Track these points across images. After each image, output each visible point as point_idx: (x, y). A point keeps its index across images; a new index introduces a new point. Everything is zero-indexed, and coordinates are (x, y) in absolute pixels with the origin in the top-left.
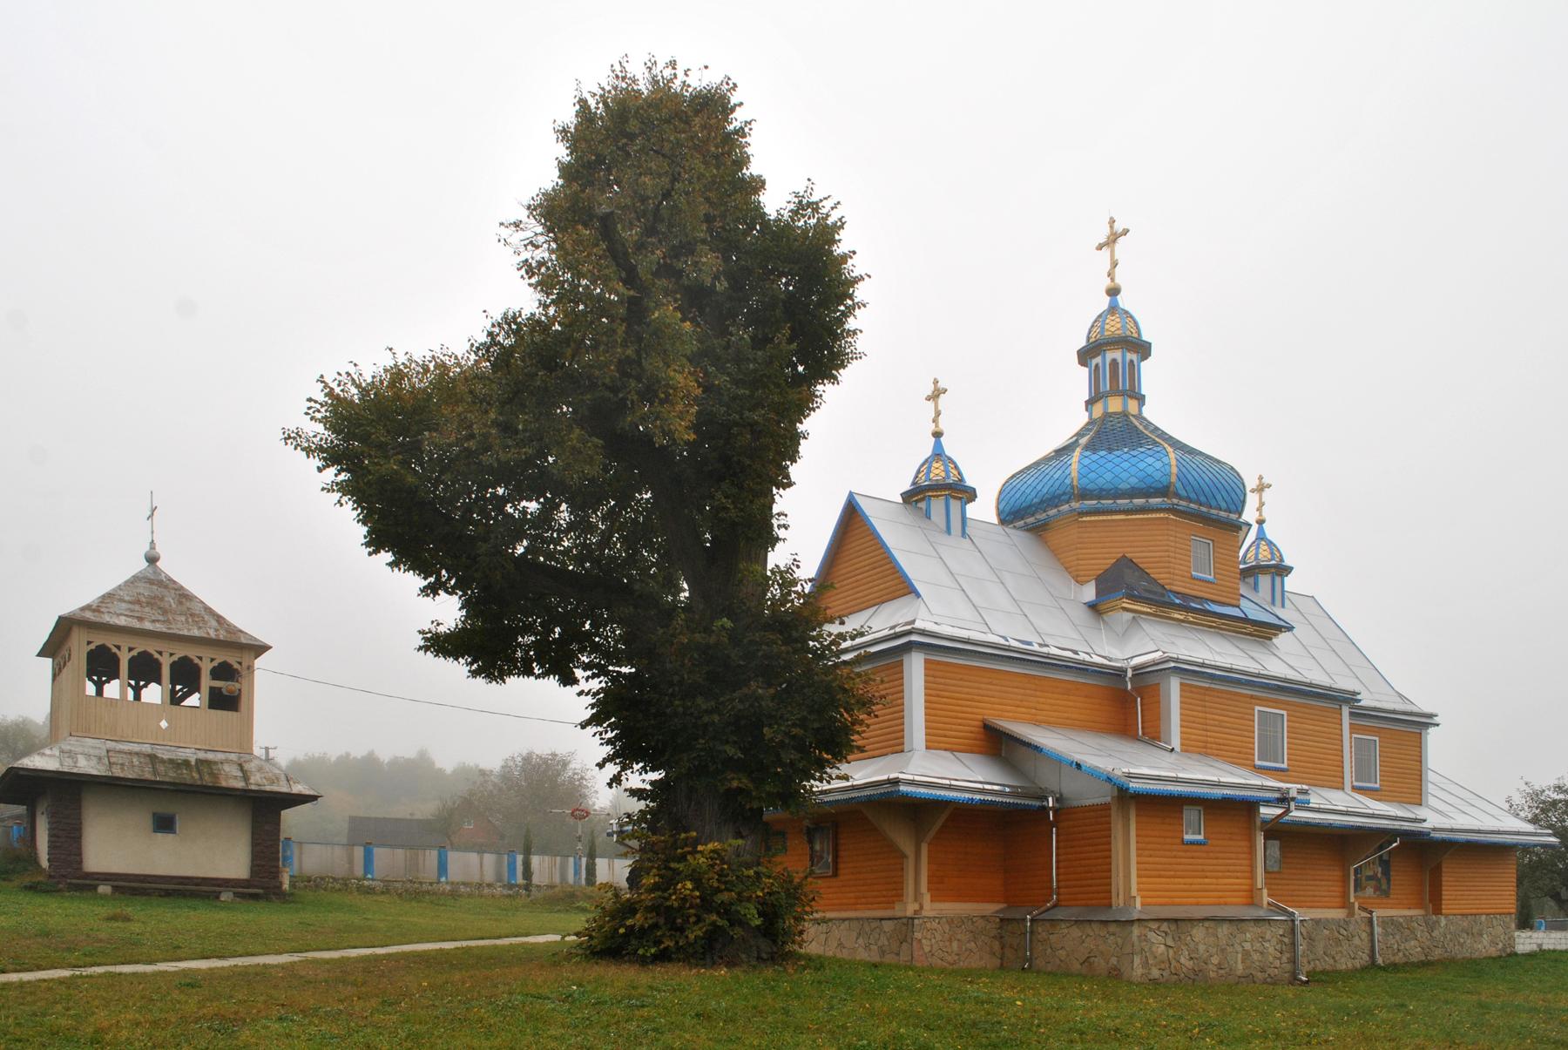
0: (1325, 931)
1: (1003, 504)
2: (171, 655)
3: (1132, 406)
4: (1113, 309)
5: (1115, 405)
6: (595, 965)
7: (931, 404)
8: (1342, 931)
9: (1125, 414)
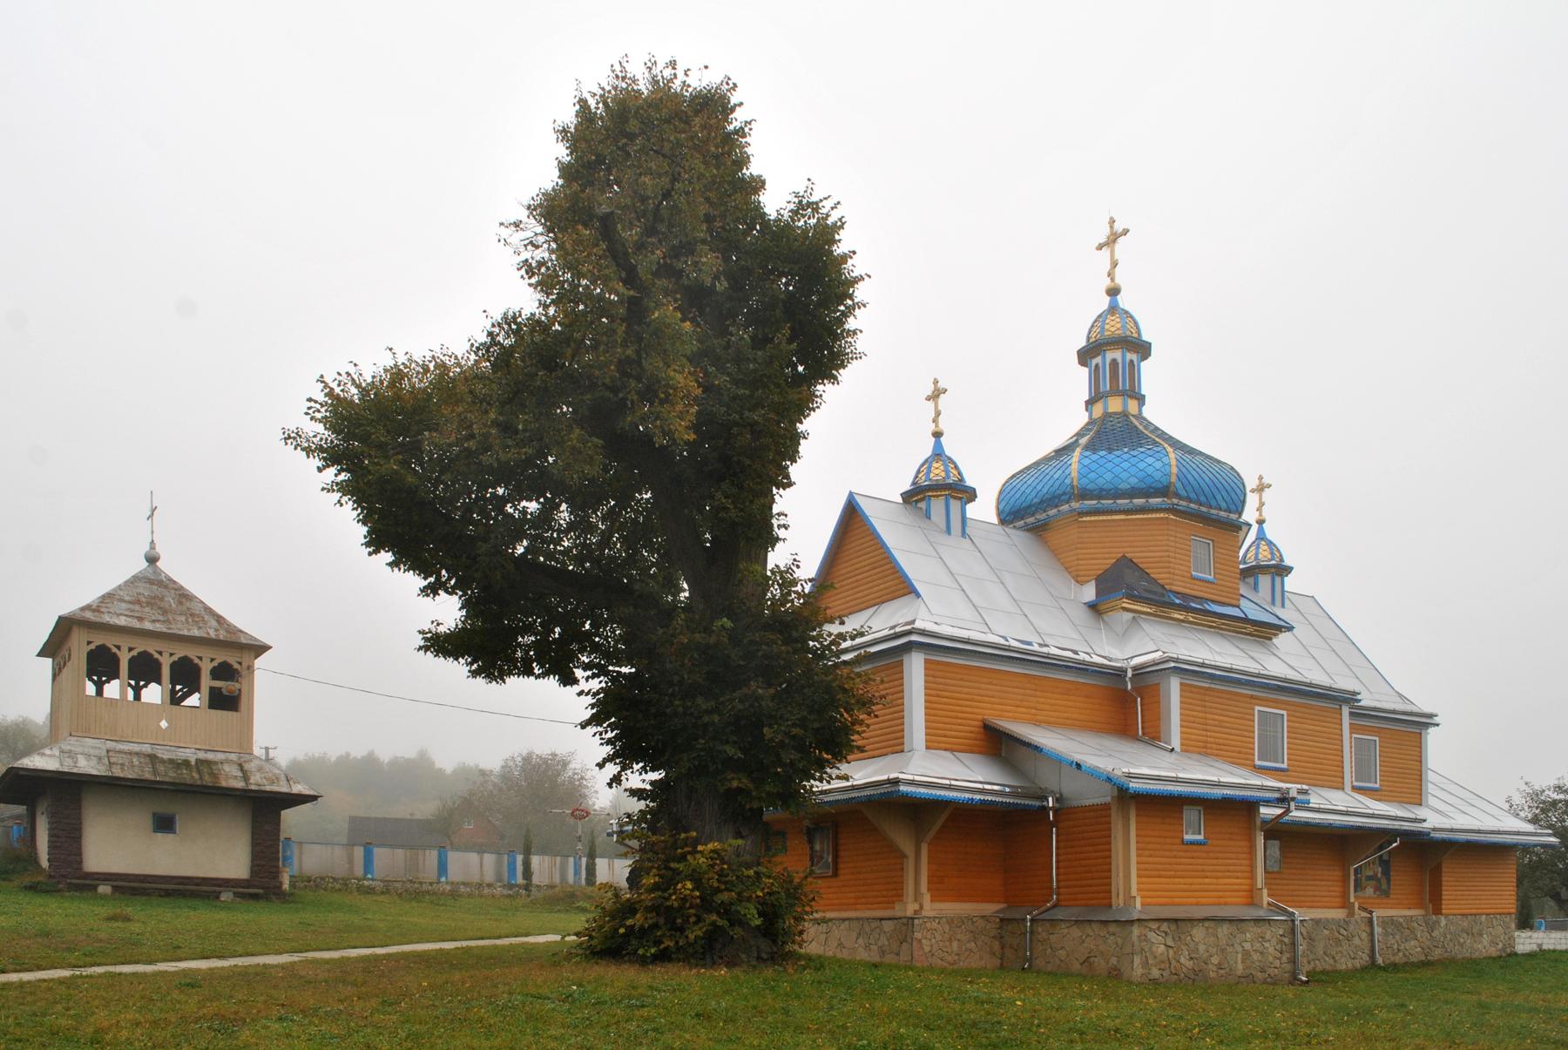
0: (1325, 931)
1: (1003, 504)
2: (171, 655)
3: (1132, 406)
4: (1113, 309)
5: (1115, 405)
6: (595, 965)
7: (931, 404)
8: (1342, 931)
9: (1125, 414)
